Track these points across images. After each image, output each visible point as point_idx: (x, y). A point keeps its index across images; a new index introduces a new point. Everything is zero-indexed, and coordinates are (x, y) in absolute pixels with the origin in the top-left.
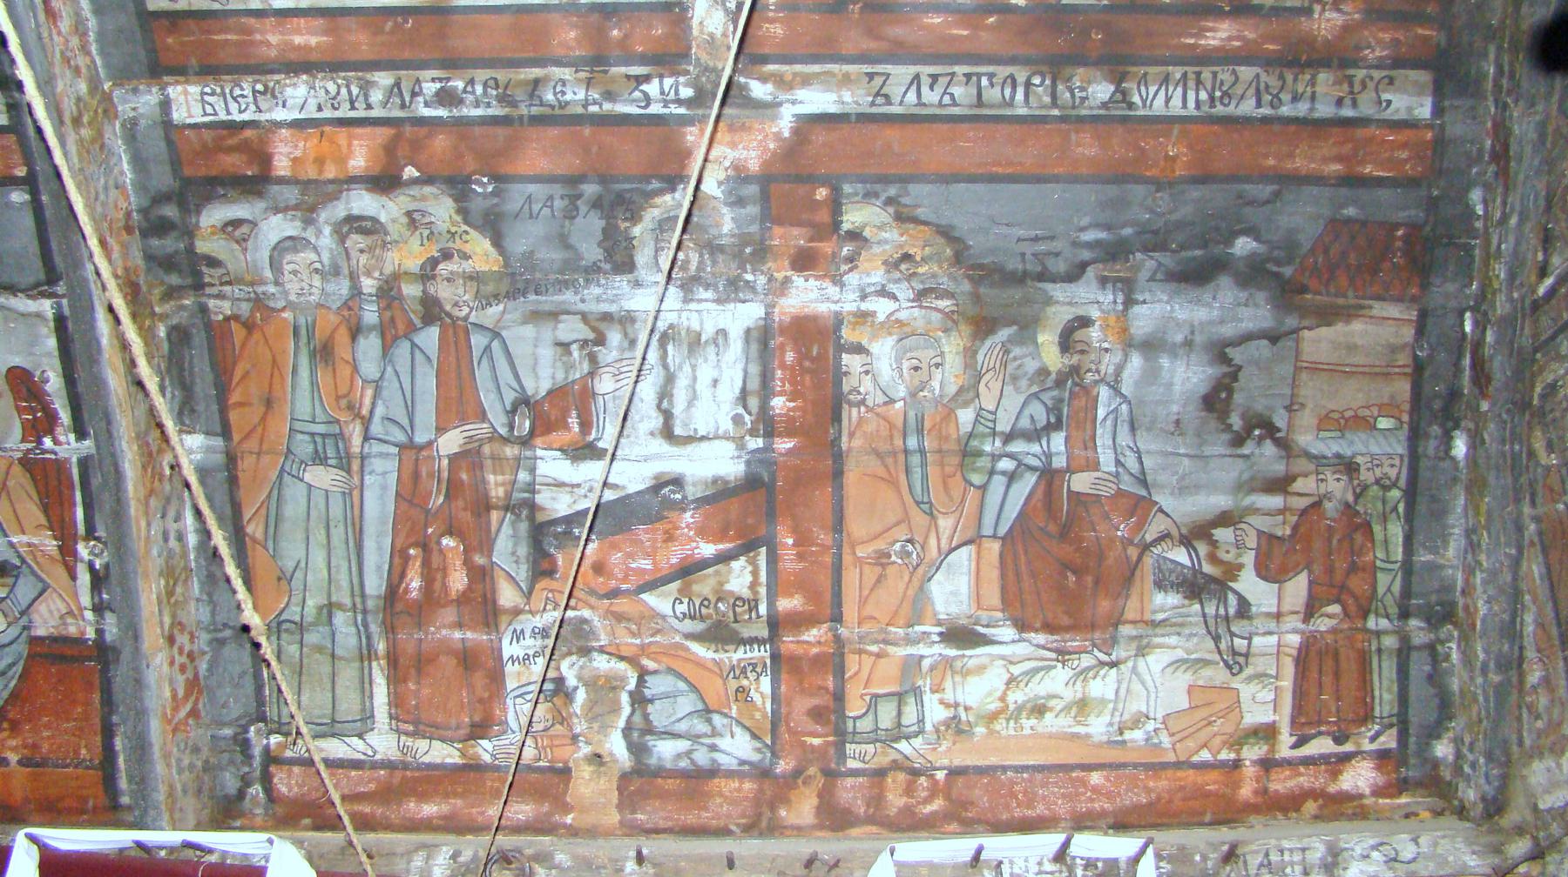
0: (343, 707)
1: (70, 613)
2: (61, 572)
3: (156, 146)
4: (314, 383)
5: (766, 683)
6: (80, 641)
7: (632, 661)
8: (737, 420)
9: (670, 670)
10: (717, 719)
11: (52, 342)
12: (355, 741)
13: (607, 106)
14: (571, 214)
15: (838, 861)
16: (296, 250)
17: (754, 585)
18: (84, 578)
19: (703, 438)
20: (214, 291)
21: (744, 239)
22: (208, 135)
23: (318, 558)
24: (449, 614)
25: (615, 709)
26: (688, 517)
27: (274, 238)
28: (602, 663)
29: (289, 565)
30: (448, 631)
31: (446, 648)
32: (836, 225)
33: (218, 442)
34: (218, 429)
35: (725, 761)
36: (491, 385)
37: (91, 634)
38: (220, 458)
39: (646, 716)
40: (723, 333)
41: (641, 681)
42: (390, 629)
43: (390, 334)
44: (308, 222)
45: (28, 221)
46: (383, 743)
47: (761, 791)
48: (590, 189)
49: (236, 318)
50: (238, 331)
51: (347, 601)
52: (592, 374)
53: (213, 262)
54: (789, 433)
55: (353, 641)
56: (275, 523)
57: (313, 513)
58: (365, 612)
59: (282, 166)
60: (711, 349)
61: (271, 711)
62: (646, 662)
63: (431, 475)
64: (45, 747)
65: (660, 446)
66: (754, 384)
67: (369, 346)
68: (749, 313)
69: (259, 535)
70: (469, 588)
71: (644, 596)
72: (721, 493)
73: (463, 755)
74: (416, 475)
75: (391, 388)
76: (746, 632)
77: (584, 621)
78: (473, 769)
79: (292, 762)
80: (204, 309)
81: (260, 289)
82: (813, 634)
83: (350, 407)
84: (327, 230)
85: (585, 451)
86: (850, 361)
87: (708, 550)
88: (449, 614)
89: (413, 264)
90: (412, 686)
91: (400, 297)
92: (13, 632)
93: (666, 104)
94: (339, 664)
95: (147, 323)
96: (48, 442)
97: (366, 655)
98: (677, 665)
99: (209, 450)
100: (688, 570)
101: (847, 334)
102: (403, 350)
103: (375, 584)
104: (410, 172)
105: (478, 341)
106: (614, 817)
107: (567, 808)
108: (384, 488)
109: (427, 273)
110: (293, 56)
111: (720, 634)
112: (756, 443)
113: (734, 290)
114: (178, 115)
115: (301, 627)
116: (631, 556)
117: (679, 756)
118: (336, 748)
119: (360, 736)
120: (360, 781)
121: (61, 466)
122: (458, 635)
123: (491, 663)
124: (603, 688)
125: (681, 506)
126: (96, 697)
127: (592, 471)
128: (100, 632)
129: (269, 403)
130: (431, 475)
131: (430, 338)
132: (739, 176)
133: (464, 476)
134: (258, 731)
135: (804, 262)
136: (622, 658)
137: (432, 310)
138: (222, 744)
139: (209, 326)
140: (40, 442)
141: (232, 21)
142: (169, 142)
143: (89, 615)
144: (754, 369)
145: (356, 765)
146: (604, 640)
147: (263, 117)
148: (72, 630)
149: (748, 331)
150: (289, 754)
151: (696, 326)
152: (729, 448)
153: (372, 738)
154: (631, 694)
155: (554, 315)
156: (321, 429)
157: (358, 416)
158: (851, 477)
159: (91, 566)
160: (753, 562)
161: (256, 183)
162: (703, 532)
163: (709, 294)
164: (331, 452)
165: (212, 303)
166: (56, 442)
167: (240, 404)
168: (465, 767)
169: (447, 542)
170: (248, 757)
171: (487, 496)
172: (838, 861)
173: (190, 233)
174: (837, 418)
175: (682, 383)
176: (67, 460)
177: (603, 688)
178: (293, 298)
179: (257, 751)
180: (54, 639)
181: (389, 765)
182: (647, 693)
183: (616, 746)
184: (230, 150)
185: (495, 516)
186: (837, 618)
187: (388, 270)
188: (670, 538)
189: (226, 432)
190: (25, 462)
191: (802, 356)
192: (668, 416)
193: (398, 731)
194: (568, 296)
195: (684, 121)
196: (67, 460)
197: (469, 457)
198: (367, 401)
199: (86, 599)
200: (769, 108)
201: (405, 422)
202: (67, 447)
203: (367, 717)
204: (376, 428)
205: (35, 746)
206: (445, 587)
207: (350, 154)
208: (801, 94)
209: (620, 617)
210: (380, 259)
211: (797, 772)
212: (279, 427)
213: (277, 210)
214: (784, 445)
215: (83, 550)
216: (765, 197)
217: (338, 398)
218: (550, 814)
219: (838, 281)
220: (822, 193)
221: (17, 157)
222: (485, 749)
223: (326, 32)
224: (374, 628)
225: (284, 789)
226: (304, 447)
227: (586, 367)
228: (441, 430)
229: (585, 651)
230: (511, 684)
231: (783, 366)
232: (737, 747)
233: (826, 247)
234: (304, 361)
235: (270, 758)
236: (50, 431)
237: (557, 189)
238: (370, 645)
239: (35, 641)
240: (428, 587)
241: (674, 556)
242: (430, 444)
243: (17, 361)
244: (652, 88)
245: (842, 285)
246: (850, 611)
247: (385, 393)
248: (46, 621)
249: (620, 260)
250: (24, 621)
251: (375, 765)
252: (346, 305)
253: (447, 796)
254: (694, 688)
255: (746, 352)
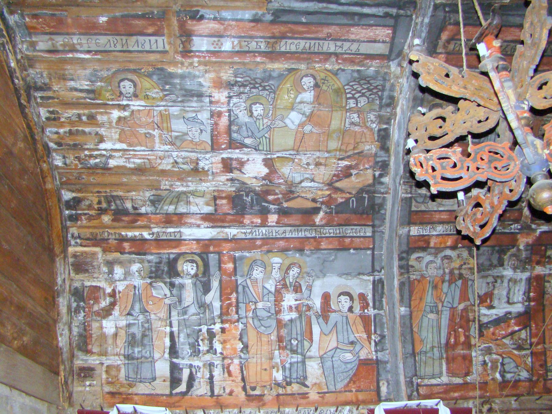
0: (435, 371)
1: (369, 353)
2: (368, 343)
3: (405, 241)
4: (432, 294)
5: (530, 359)
6: (371, 360)
7: (501, 355)
8: (523, 299)
9: (509, 357)
10: (519, 368)
11: (371, 287)
12: (438, 379)
13: (503, 230)
14: (492, 254)
15: (101, 406)
16: (432, 263)
17: (526, 336)
18: (373, 343)
19: (516, 303)
20: (412, 273)
21: (526, 258)
22: (417, 238)
23: (430, 336)
24: (460, 347)
25: (497, 367)
26: (513, 321)
27: (428, 260)
28: (494, 356)
29: (423, 337)
30: (460, 351)
31: (459, 355)
32: (545, 254)
33: (408, 309)
34: (408, 306)
35: (522, 378)
36: (471, 293)
37: (375, 358)
38: (408, 313)
39: (504, 368)
40: (521, 279)
41: (503, 360)
42: (446, 351)
43: (451, 282)
44: (436, 257)
45: (370, 258)
46: (445, 379)
47: (530, 384)
48: (497, 248)
49: (416, 279)
50: (416, 282)
51: (437, 345)
52: (493, 289)
53: (412, 267)
54: (533, 301)
55: (438, 355)
56: (420, 327)
57: (430, 325)
58: (441, 348)
59: (432, 245)
60: (518, 283)
61: (418, 373)
62: (504, 356)
63: (457, 314)
64: (362, 387)
65: (506, 305)
66: (527, 290)
67: (446, 285)
68: (526, 275)
69: (417, 331)
70: (465, 341)
71: (503, 340)
72: (520, 315)
73: (464, 380)
74: (453, 315)
75: (449, 294)
76: (525, 347)
77: (490, 346)
78: (466, 383)
79: (423, 386)
80: (409, 278)
81: (422, 273)
82: (539, 347)
83: (440, 299)
84: (439, 259)
85: (491, 307)
86: (547, 284)
87: (517, 328)
88: (460, 347)
89: (457, 266)
90: (452, 365)
91: (454, 273)
92: (355, 358)
93: (514, 229)
94: (435, 361)
95: (140, 203)
96: (366, 311)
97: (441, 358)
98: (511, 356)
99: (406, 311)
100: (513, 333)
101: (546, 278)
102: (453, 285)
103: (443, 341)
104: (460, 245)
105: (470, 283)
106: (498, 393)
107: (487, 392)
108: (446, 318)
109: (460, 268)
110: (441, 220)
111: (520, 348)
112: (527, 303)
113: (524, 270)
114: (412, 233)
115: (426, 352)
116: (500, 331)
117: (511, 377)
118: (434, 381)
119: (439, 378)
120: (440, 389)
121: (369, 317)
122: (462, 352)
123: (469, 358)
124: (494, 362)
125: (511, 319)
126: (375, 373)
127: (493, 311)
128: (377, 357)
129: (421, 299)
130: (457, 314)
131: (459, 283)
132: (527, 245)
133: (464, 314)
134: (415, 379)
135: (538, 263)
136: (498, 355)
137: (461, 276)
138: (113, 373)
139: (410, 281)
140: (364, 311)
141: (429, 213)
142: (408, 239)
143: (374, 353)
144: (527, 287)
145: (438, 385)
146: (495, 351)
147: (430, 234)
148: (370, 357)
149: (526, 279)
150: (423, 384)
151: (516, 278)
152: (520, 305)
153: (443, 378)
154: (501, 363)
155: (487, 277)
156: (432, 305)
157: (441, 301)
158: (547, 310)
159: (375, 341)
160: (526, 331)
161: (424, 249)
162: (516, 324)
163: (519, 271)
164: (434, 310)
165: (411, 276)
166: (368, 311)
167: (415, 300)
168: (464, 384)
169: (460, 330)
170: (413, 385)
171: (469, 318)
172: (101, 406)
173: (408, 260)
174: (543, 297)
175: (512, 290)
176: (371, 315)
177: (494, 362)
178: (430, 274)
179: (415, 384)
180: (365, 360)
181: (446, 384)
182: (504, 363)
183: (498, 376)
184: (421, 241)
185: (471, 323)
186: (544, 343)
187: (452, 267)
188: (509, 326)
189: (410, 307)
190: (360, 316)
191: (537, 283)
192: (508, 298)
193: (448, 376)
194: (490, 272)
195: (518, 233)
196: (371, 315)
197: (465, 310)
198: (444, 298)
199: (373, 349)
200: (535, 230)
201: (451, 302)
202: (371, 312)
203: (441, 373)
204: (445, 304)
205: (359, 387)
206: (459, 340)
207: (448, 241)
208: (542, 227)
209: (498, 345)
210: (450, 265)
211: (538, 380)
212: (423, 305)
213: (429, 254)
214: (532, 304)
215: (373, 337)
216: (532, 249)
217: (437, 297)
218: (483, 394)
219: (544, 266)
220: (543, 248)
221: (371, 243)
222: (468, 379)
223: (449, 215)
224: (443, 351)
225: (421, 392)
226: (428, 309)
227: (492, 288)
228: (459, 304)
229: (490, 354)
230: (474, 363)
231: (533, 286)
232: (524, 374)
233: (543, 260)
234: (430, 289)
235: (418, 385)
236: (367, 308)
237: (490, 249)
238: (442, 355)
239: (360, 360)
240: (455, 341)
241: (510, 330)
242: (457, 307)
243: (362, 291)
244: (512, 227)
245: (546, 268)
246: (547, 341)
247: (448, 296)
248: (363, 355)
249: (501, 264)
250: (357, 355)
251: (443, 385)
252: (442, 276)
253: (460, 391)
254: (514, 361)
255: (526, 283)
